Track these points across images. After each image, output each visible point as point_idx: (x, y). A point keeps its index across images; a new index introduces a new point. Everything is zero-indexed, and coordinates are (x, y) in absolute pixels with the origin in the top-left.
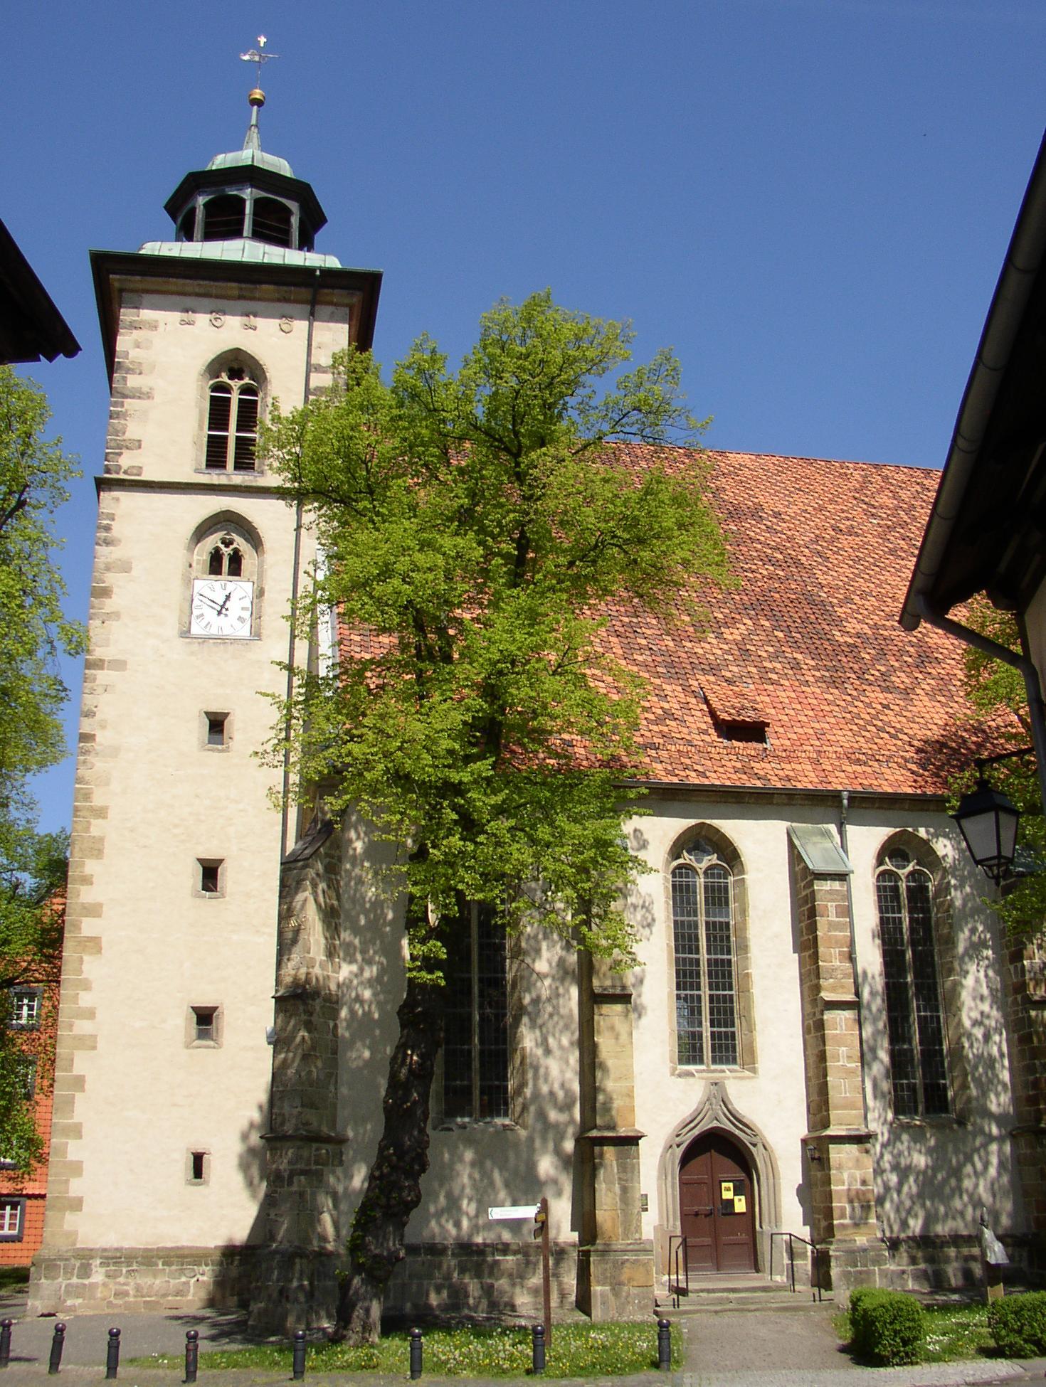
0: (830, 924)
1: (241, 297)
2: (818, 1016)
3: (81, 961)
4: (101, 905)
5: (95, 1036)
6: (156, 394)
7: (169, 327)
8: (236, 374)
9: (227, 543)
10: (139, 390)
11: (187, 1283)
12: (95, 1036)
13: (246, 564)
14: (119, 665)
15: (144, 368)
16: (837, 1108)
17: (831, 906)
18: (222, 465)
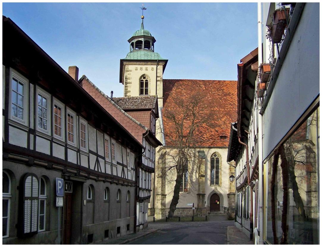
8: (144, 78)
15: (130, 78)
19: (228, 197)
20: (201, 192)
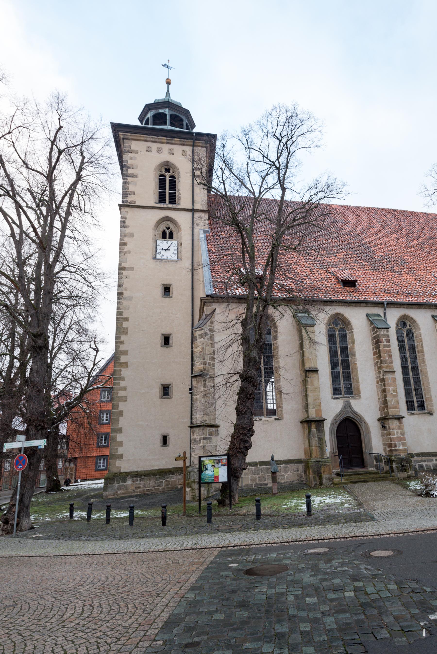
0: (384, 345)
1: (168, 143)
2: (382, 377)
3: (121, 371)
4: (127, 351)
5: (126, 397)
6: (139, 176)
7: (142, 153)
8: (168, 170)
9: (168, 228)
10: (133, 174)
11: (162, 482)
12: (126, 397)
13: (175, 235)
14: (132, 269)
15: (134, 167)
16: (390, 408)
17: (384, 339)
18: (164, 202)
19: (384, 427)
20: (313, 414)
